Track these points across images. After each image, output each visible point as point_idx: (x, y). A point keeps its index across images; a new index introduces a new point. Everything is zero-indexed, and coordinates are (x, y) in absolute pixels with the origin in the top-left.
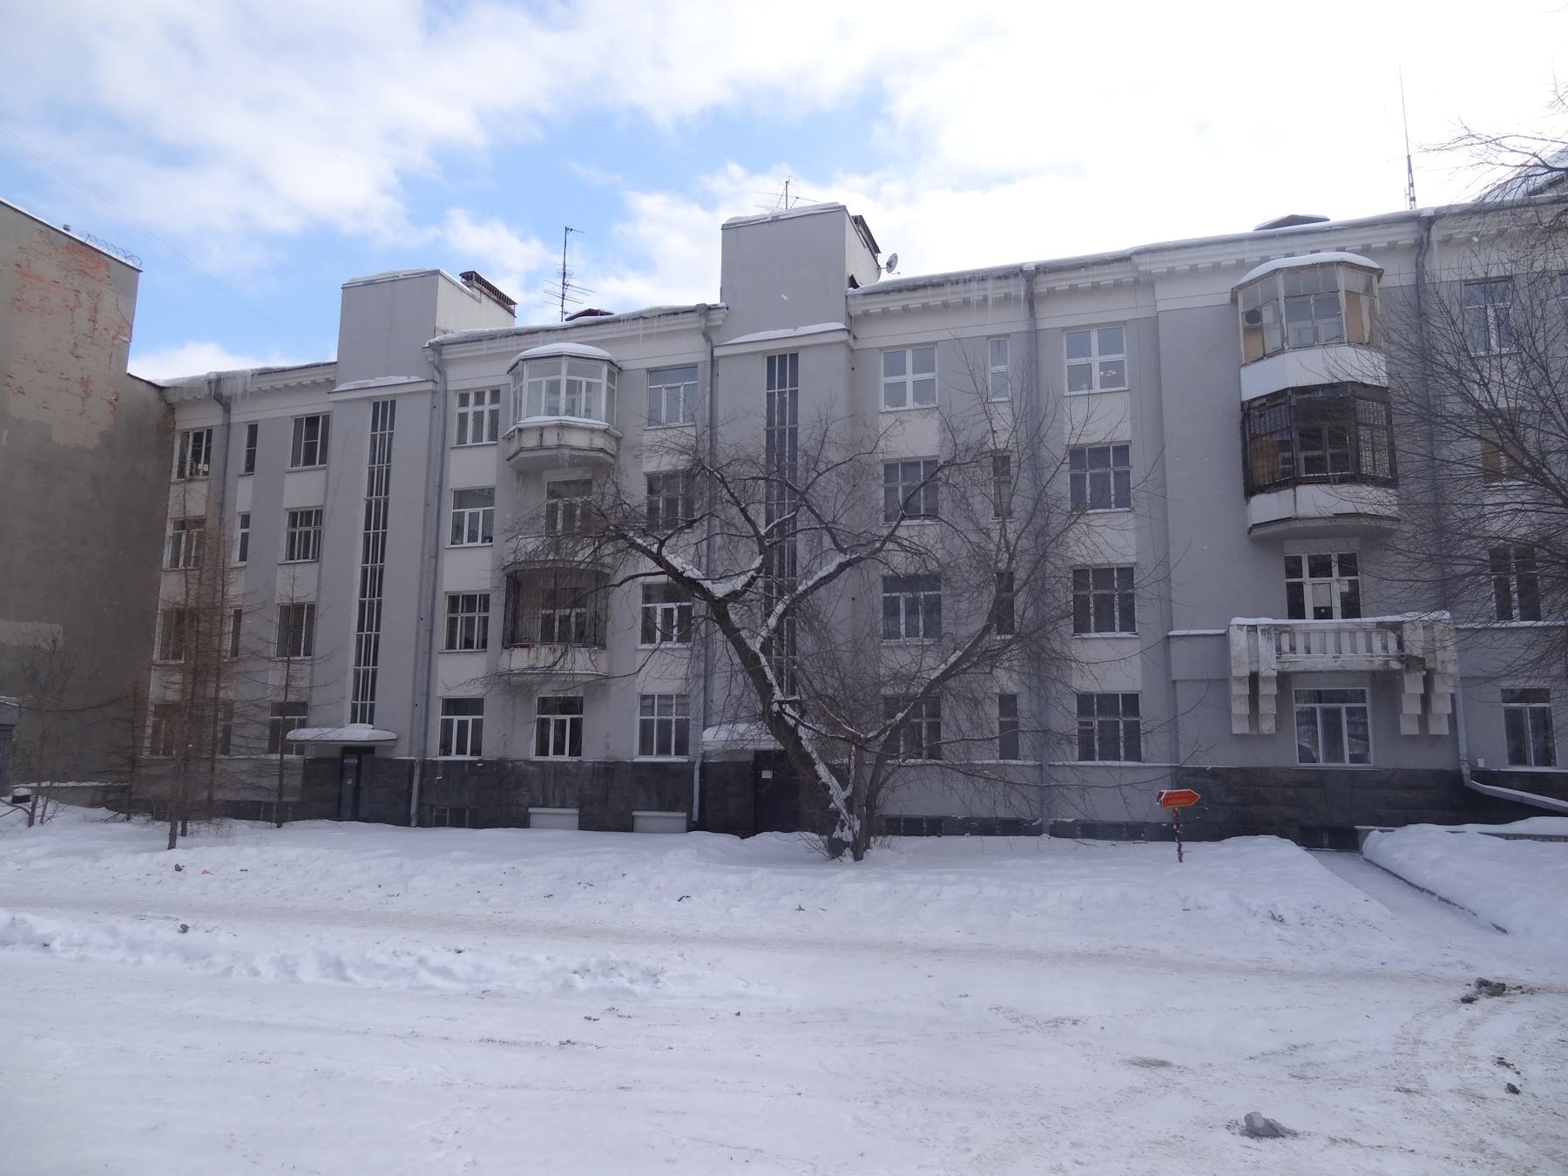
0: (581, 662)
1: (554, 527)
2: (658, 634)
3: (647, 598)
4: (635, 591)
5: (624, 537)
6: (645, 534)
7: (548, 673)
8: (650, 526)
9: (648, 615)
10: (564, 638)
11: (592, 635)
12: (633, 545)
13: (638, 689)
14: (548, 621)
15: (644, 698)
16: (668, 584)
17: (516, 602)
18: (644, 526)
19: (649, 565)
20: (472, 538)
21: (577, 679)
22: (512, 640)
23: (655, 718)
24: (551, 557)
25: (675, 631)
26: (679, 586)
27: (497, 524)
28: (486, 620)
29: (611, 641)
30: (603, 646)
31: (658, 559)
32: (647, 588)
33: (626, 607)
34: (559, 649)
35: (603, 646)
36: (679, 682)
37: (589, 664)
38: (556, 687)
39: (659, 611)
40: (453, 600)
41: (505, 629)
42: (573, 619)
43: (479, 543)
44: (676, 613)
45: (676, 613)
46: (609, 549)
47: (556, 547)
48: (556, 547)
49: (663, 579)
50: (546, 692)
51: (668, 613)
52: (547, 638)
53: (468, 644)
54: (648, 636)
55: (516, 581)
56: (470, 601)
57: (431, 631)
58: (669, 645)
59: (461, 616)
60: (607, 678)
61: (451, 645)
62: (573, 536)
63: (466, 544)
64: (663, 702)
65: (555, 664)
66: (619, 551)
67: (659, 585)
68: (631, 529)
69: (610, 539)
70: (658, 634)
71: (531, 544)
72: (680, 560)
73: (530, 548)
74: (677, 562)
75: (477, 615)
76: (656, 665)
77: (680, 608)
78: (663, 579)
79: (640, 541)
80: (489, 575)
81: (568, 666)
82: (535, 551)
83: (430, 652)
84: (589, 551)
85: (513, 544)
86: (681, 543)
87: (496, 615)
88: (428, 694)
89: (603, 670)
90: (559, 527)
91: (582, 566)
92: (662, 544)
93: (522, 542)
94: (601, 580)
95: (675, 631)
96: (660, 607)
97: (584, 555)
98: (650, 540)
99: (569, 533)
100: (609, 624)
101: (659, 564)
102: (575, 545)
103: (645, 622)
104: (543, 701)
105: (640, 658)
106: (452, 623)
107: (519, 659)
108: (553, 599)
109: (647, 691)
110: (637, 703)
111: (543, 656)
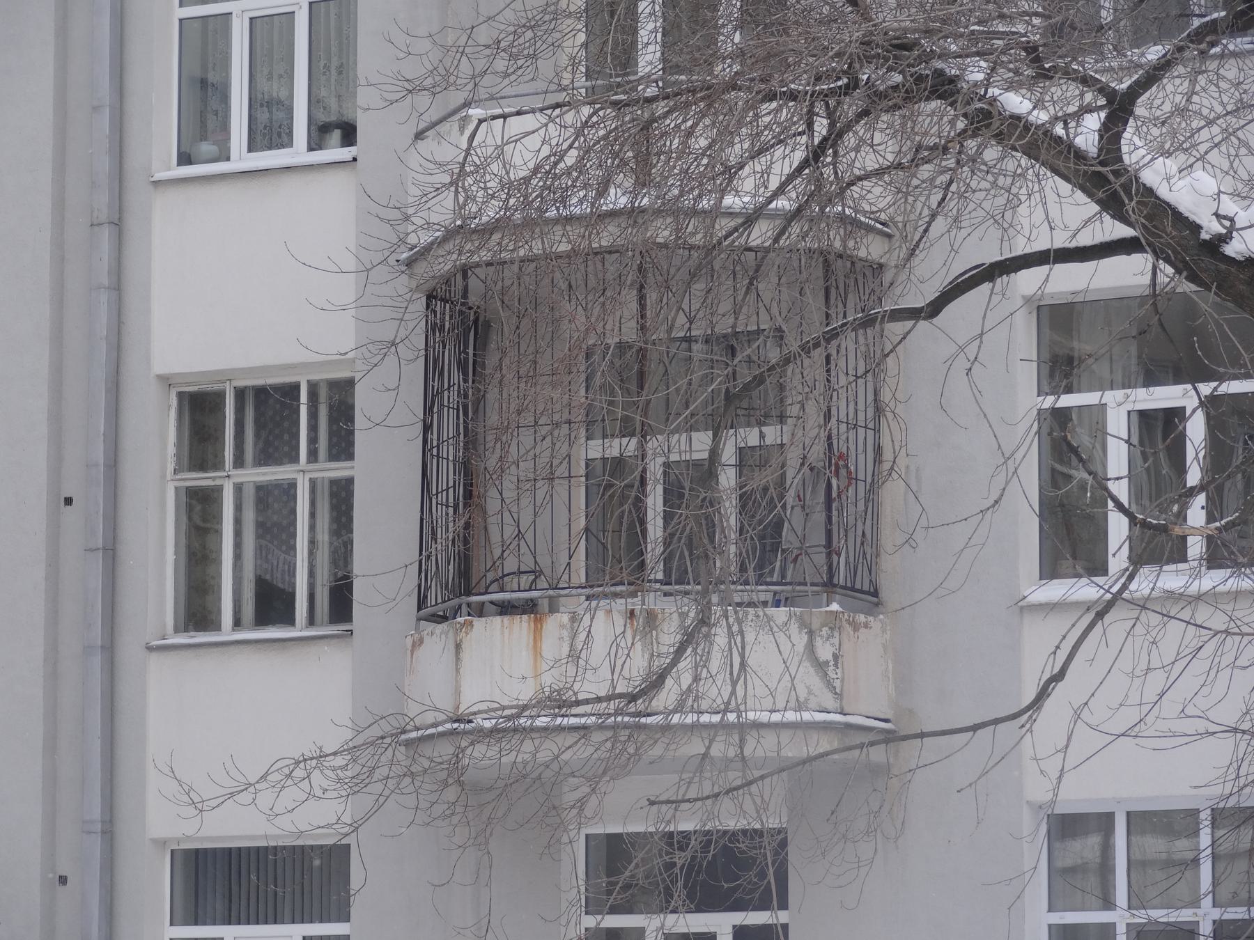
0: (773, 669)
1: (626, 58)
2: (1118, 527)
3: (1061, 368)
4: (1002, 330)
5: (944, 88)
6: (1039, 66)
7: (630, 720)
8: (1056, 31)
9: (1064, 442)
10: (687, 566)
11: (813, 542)
12: (987, 121)
13: (1038, 790)
14: (615, 488)
15: (1066, 826)
16: (1154, 296)
17: (472, 408)
18: (1033, 29)
19: (1069, 213)
20: (270, 132)
21: (761, 748)
22: (461, 582)
23: (1120, 918)
24: (617, 198)
25: (1196, 514)
26: (1207, 302)
27: (373, 59)
28: (341, 497)
29: (893, 570)
30: (868, 596)
31: (1106, 181)
32: (1058, 318)
33: (965, 411)
34: (673, 614)
35: (868, 596)
36: (1222, 750)
37: (808, 678)
38: (664, 785)
39: (1118, 424)
40: (199, 408)
41: (427, 533)
42: (727, 478)
43: (298, 152)
44: (1196, 430)
45: (1196, 430)
46: (875, 145)
47: (640, 152)
48: (640, 152)
49: (1130, 274)
50: (625, 811)
51: (1159, 429)
52: (617, 559)
53: (272, 604)
54: (1070, 537)
55: (466, 322)
56: (271, 410)
57: (111, 552)
58: (1172, 579)
59: (235, 480)
60: (890, 738)
61: (197, 612)
62: (711, 94)
63: (241, 158)
64: (1155, 846)
65: (656, 682)
66: (921, 154)
67: (1111, 307)
68: (978, 47)
69: (877, 101)
70: (1118, 527)
71: (526, 142)
72: (1206, 181)
73: (524, 158)
74: (1193, 191)
75: (304, 475)
76: (1113, 670)
77: (1211, 404)
78: (1130, 274)
79: (1016, 102)
80: (346, 289)
81: (716, 690)
82: (546, 170)
83: (110, 649)
84: (785, 161)
85: (447, 147)
86: (1207, 102)
87: (387, 468)
88: (109, 832)
89: (870, 701)
90: (649, 58)
91: (760, 234)
92: (1120, 110)
93: (490, 135)
94: (849, 293)
95: (1196, 514)
96: (1120, 407)
97: (764, 178)
98: (1067, 93)
99: (694, 90)
100: (892, 494)
101: (1112, 205)
102: (725, 136)
103: (1053, 479)
104: (612, 853)
105: (1038, 647)
106: (199, 509)
107: (497, 664)
108: (632, 384)
109: (1078, 795)
110: (1034, 853)
111: (595, 647)
